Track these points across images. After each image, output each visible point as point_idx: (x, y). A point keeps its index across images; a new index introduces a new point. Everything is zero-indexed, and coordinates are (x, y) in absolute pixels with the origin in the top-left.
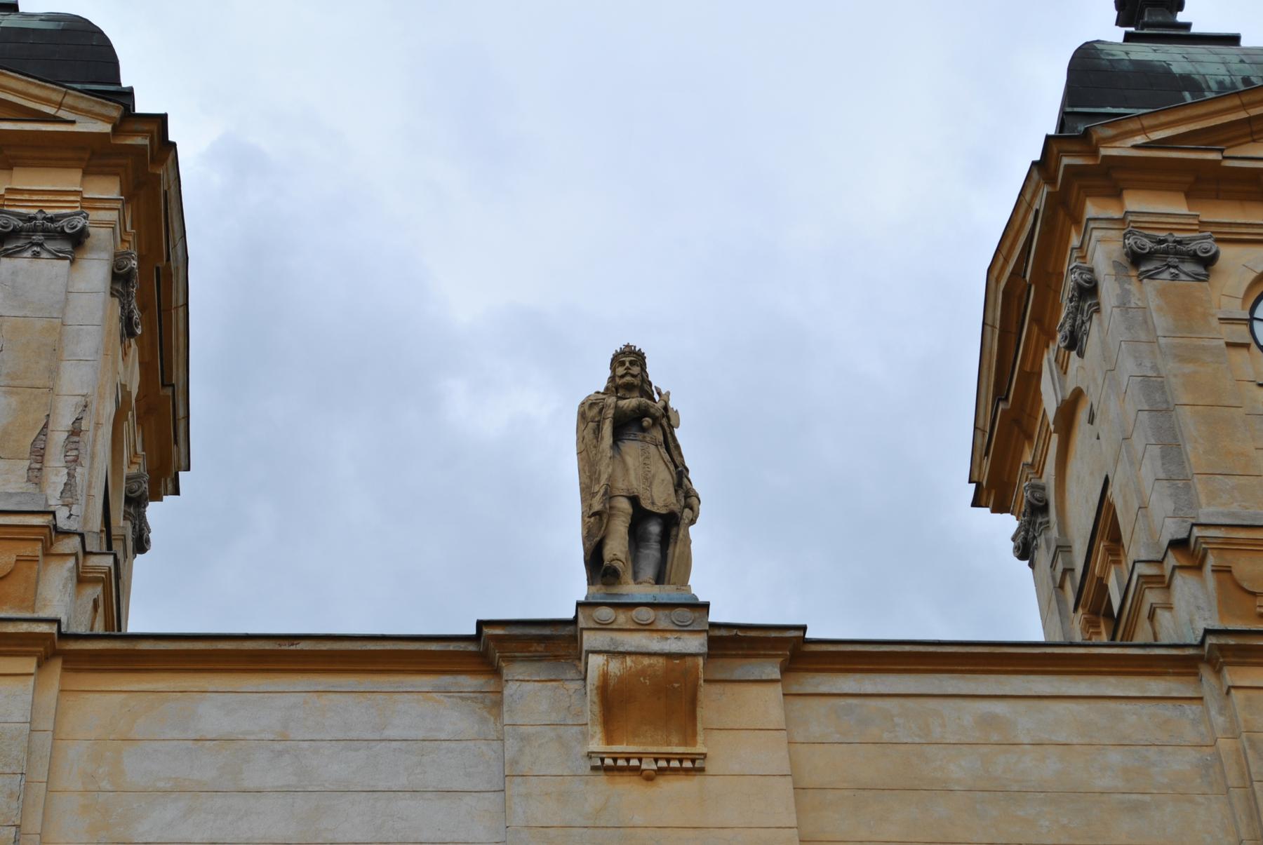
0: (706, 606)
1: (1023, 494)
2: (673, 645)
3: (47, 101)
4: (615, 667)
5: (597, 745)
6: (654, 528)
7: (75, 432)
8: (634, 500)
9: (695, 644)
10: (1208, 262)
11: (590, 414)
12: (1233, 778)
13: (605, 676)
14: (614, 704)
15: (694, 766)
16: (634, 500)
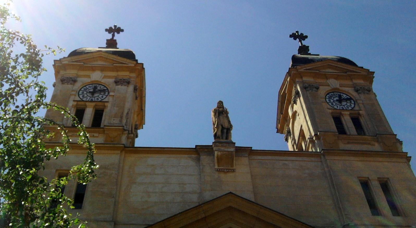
0: (235, 143)
1: (286, 130)
2: (229, 150)
3: (124, 61)
4: (219, 153)
5: (216, 167)
6: (225, 131)
7: (128, 114)
8: (222, 126)
9: (232, 149)
10: (318, 88)
11: (215, 111)
12: (328, 175)
13: (218, 155)
14: (219, 160)
15: (234, 171)
16: (222, 126)
